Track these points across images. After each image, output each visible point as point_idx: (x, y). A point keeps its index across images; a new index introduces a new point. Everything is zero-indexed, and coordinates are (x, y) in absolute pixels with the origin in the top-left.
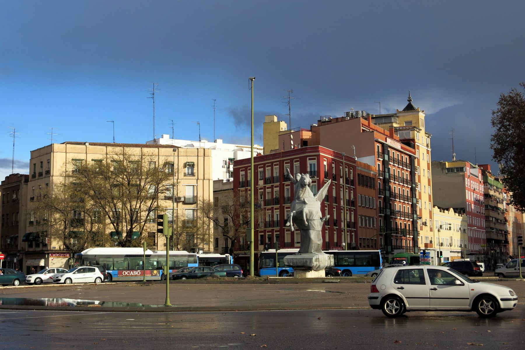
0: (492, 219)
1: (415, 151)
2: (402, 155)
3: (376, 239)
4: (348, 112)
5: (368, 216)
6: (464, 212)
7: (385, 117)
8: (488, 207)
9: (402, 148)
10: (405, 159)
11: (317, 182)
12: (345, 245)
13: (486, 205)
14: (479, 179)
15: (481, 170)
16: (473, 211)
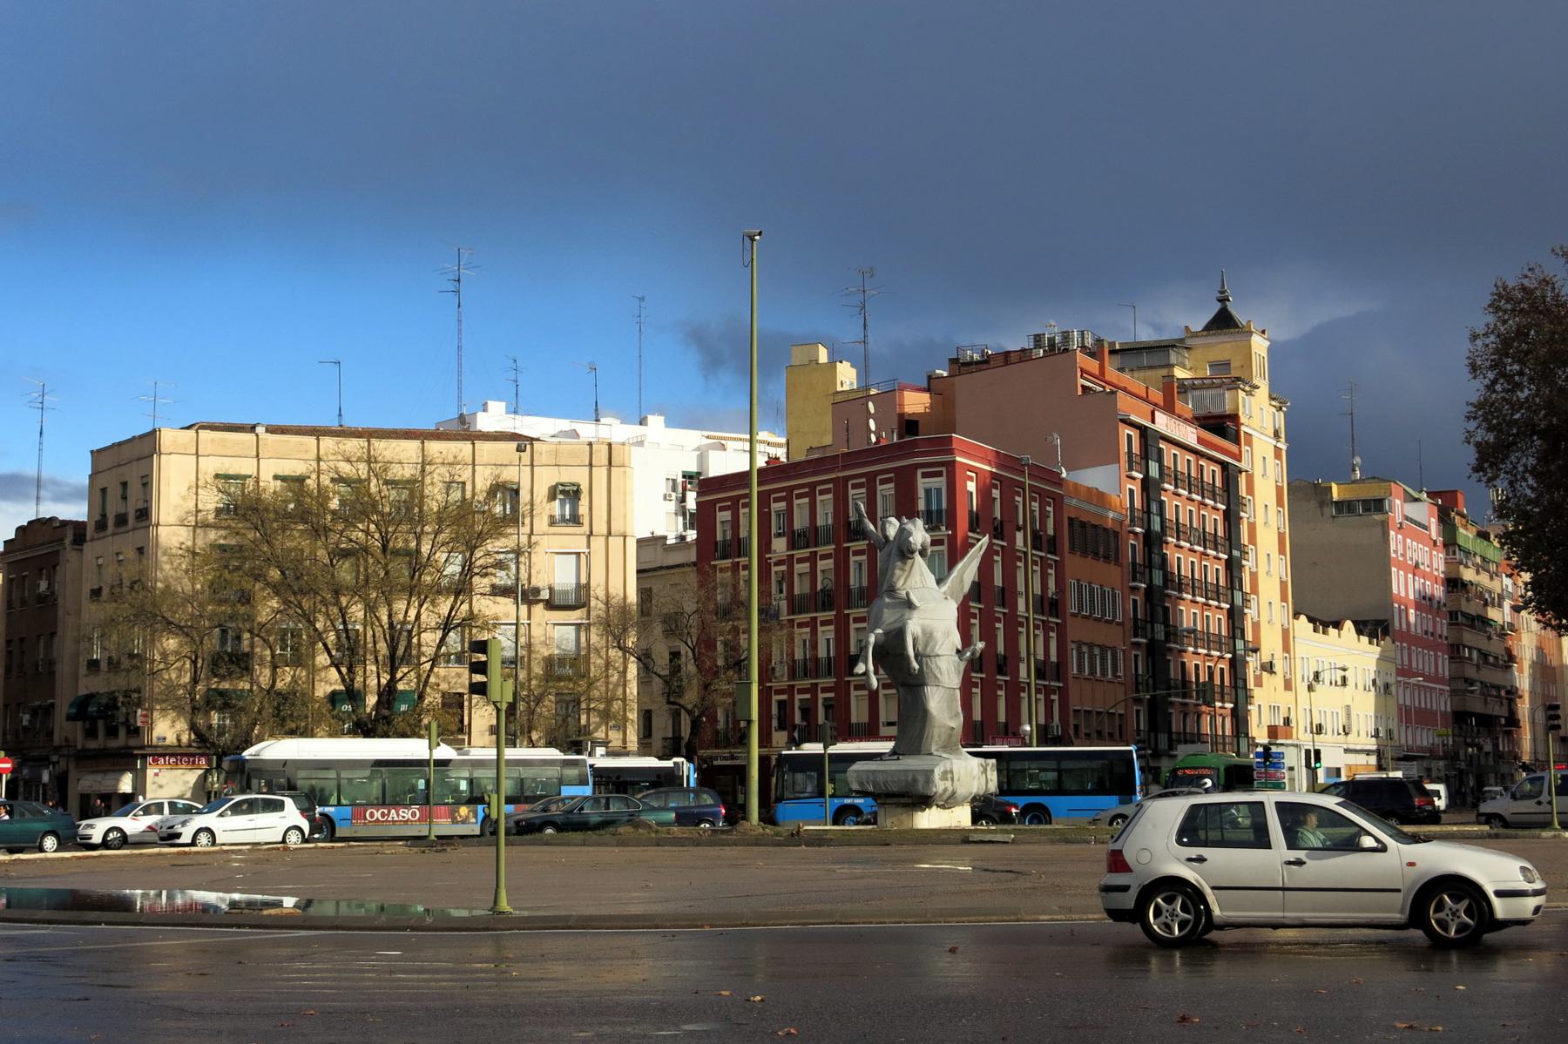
0: (1470, 653)
1: (1240, 452)
2: (1200, 463)
3: (1122, 712)
4: (1039, 335)
5: (1098, 646)
6: (1386, 632)
7: (1149, 348)
8: (1457, 619)
9: (1200, 440)
10: (1208, 473)
11: (946, 542)
12: (1031, 731)
13: (1450, 613)
14: (1430, 535)
15: (1436, 508)
16: (1413, 629)
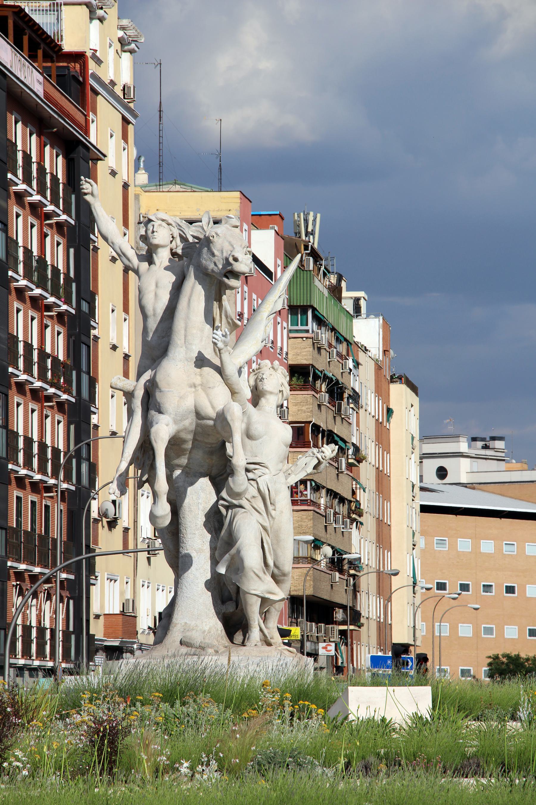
1: (87, 122)
